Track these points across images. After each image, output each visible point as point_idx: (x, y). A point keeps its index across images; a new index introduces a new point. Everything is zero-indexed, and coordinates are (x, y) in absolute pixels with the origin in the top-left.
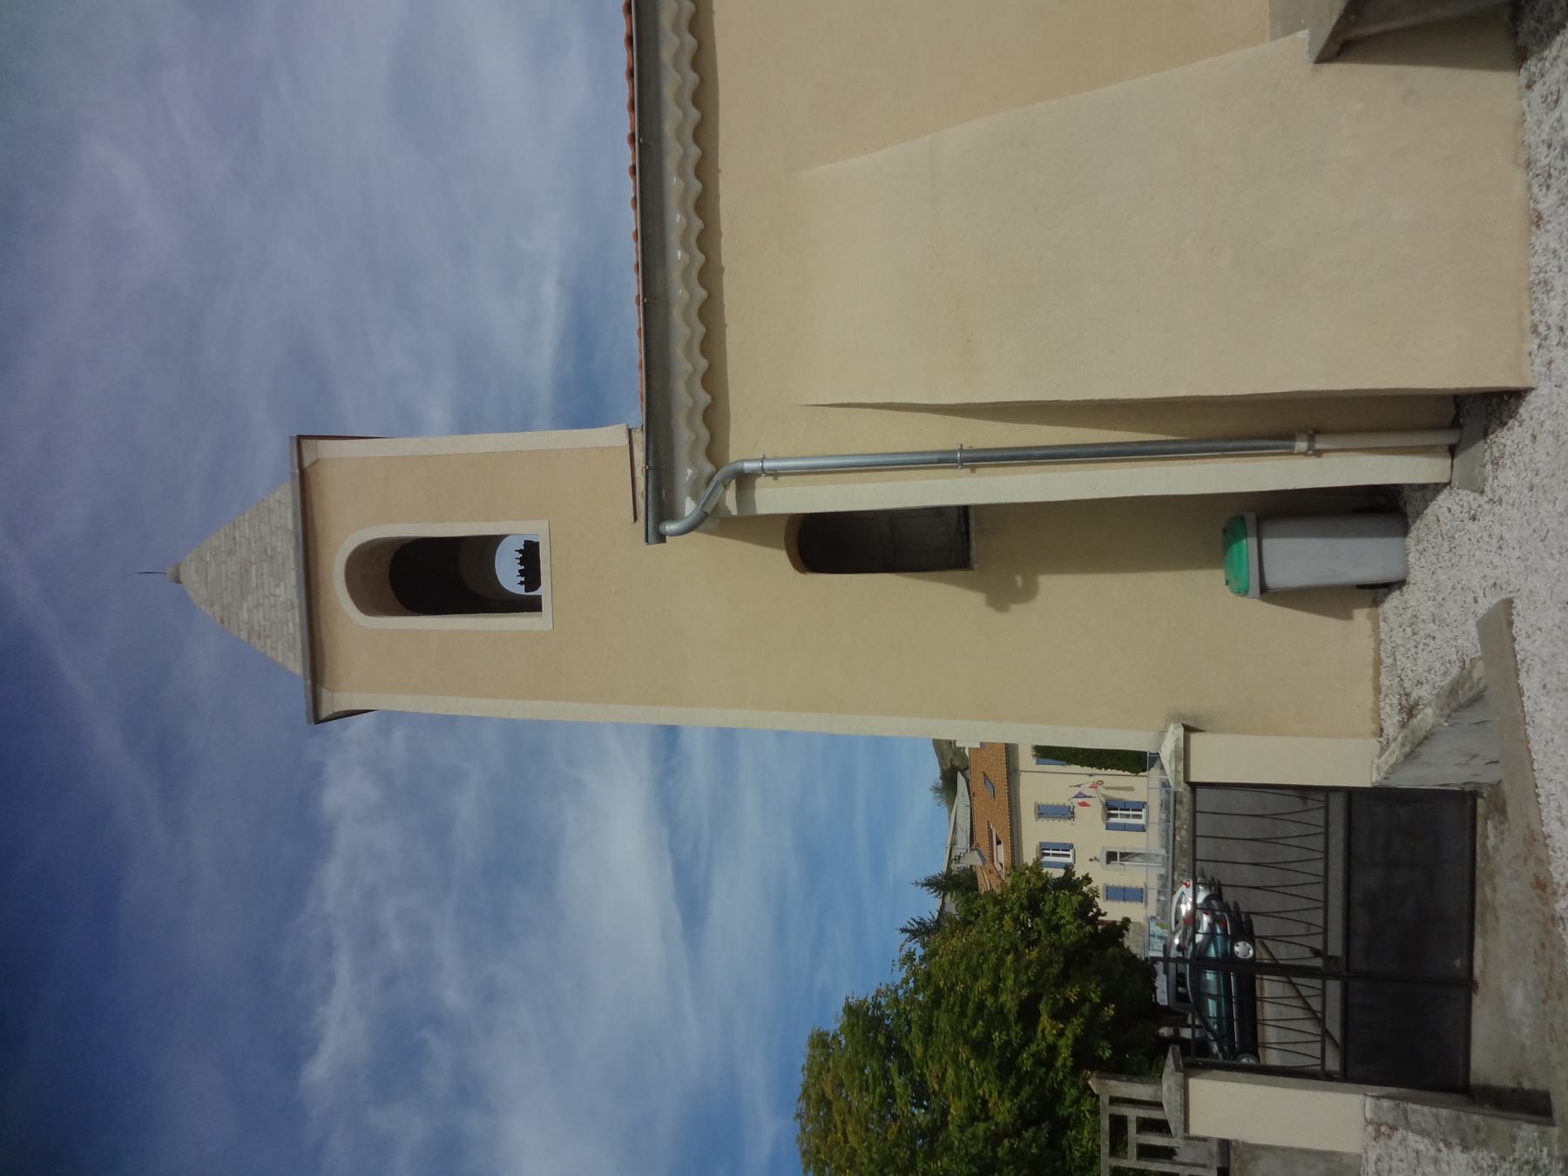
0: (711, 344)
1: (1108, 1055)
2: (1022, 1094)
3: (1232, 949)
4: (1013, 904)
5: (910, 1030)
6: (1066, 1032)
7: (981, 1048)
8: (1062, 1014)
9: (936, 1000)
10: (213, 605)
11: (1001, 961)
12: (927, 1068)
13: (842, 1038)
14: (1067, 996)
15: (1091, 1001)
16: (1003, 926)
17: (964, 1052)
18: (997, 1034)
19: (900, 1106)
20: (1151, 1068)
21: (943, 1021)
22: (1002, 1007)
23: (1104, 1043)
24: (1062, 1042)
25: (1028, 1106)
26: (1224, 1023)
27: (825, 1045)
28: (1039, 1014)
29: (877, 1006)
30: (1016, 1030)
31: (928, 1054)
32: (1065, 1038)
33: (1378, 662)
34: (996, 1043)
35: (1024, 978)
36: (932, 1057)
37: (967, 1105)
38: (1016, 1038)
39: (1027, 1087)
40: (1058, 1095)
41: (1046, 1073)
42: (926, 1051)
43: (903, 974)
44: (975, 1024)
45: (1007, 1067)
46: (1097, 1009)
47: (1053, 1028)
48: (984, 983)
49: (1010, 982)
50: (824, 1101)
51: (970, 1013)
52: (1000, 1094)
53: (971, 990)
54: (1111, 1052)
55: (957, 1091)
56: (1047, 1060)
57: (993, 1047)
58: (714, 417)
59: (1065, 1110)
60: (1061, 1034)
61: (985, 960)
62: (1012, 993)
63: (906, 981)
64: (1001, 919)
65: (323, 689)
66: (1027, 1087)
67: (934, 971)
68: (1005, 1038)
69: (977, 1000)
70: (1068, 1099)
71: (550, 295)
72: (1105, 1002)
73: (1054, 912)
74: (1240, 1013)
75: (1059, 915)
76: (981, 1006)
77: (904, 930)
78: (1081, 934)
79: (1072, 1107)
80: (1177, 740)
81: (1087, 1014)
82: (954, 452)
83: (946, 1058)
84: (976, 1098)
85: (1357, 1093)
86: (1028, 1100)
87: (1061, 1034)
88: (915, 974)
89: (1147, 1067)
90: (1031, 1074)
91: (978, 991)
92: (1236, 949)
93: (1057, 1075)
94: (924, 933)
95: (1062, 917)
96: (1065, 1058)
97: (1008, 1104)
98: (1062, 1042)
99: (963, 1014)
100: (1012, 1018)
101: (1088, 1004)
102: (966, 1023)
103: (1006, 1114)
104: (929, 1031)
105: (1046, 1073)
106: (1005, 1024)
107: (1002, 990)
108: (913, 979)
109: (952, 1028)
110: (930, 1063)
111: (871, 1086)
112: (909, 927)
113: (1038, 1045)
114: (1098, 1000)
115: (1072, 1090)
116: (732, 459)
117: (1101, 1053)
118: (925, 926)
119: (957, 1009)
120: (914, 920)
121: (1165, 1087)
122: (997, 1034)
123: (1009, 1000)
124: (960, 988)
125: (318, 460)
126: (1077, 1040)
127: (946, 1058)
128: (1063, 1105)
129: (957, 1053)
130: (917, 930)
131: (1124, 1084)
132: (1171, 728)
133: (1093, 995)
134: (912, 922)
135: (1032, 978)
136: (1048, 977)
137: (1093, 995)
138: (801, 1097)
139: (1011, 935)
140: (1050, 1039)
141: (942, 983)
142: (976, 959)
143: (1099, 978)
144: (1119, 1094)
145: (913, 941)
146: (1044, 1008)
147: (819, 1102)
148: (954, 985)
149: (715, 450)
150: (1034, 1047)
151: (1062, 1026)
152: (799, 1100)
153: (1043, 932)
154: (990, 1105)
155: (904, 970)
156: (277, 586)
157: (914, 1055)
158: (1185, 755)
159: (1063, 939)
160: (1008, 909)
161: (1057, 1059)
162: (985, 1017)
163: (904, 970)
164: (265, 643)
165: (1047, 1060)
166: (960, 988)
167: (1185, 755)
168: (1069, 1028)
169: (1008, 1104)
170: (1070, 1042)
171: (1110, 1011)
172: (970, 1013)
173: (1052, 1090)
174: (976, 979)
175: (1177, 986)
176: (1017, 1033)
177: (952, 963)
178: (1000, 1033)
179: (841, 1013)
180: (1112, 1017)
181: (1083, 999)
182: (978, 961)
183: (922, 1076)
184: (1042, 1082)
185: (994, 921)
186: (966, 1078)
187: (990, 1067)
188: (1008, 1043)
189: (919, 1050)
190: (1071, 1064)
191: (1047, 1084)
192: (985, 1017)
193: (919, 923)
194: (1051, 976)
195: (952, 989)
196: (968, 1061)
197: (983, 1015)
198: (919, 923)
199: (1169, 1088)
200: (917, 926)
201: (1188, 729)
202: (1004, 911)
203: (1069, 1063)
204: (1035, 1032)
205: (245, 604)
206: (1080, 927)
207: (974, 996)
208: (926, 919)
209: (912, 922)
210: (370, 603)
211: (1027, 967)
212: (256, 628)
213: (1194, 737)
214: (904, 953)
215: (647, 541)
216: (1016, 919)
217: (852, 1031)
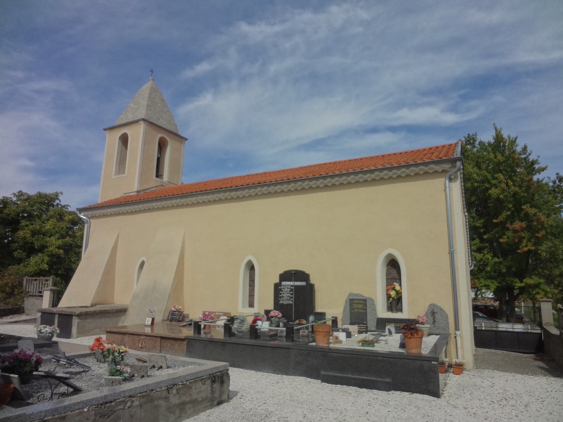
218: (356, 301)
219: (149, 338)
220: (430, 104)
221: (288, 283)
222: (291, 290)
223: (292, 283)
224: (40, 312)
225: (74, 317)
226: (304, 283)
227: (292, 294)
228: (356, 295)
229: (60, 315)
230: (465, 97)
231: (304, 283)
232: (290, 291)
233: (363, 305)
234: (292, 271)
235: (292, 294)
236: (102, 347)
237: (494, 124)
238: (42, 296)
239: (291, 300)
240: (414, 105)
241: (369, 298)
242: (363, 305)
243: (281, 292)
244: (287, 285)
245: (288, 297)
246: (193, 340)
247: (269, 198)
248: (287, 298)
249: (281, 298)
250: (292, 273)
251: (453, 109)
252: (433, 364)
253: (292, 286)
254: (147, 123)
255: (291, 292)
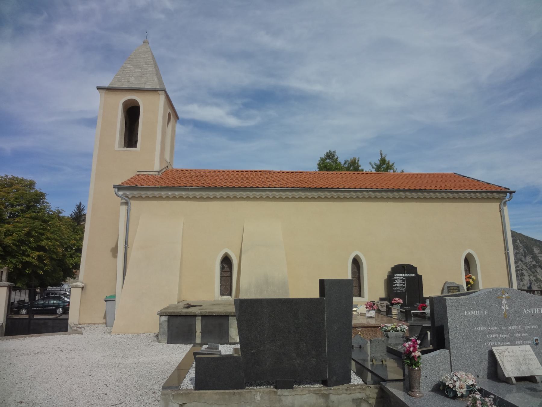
0: (154, 198)
1: (27, 272)
2: (14, 247)
3: (61, 308)
4: (80, 244)
5: (35, 212)
6: (34, 260)
7: (28, 234)
8: (40, 258)
9: (44, 221)
10: (134, 55)
11: (57, 241)
12: (22, 218)
13: (33, 191)
14: (46, 260)
15: (45, 267)
16: (72, 240)
17: (27, 230)
18: (33, 239)
19: (10, 209)
20: (23, 284)
21: (37, 223)
22: (42, 241)
23: (30, 271)
24: (30, 258)
25: (10, 248)
26: (36, 305)
27: (30, 185)
28: (39, 252)
29: (43, 203)
30: (35, 245)
31: (26, 218)
32: (32, 259)
33: (94, 324)
34: (30, 239)
35: (52, 247)
36: (25, 220)
37: (10, 230)
38: (32, 245)
39: (16, 248)
40: (14, 257)
41: (20, 254)
42: (28, 217)
43: (54, 210)
44: (36, 232)
45: (22, 242)
46: (42, 269)
47: (35, 256)
48: (50, 235)
49: (50, 243)
50: (11, 185)
51: (40, 231)
52: (14, 240)
53: (49, 232)
54: (28, 273)
55: (15, 227)
56: (24, 254)
57: (29, 238)
58: (140, 198)
59: (9, 259)
60: (33, 258)
61: (58, 236)
62: (47, 244)
63: (52, 211)
64: (75, 240)
65: (105, 91)
66: (16, 248)
67: (55, 221)
68: (32, 242)
69: (45, 233)
70: (12, 260)
71: (317, 88)
72: (44, 271)
73: (77, 256)
74: (40, 310)
75: (76, 257)
76: (42, 234)
77: (80, 204)
78: (69, 264)
79: (10, 261)
80: (80, 285)
81: (40, 266)
82: (127, 245)
83: (25, 224)
84: (13, 233)
85: (4, 321)
86: (12, 248)
87: (33, 258)
88: (54, 214)
89: (23, 283)
90: (20, 249)
91: (47, 234)
92: (60, 309)
93: (20, 257)
94: (79, 210)
95: (75, 259)
96: (25, 259)
97: (10, 242)
98: (30, 258)
99: (40, 229)
100: (39, 244)
101: (43, 266)
102: (37, 230)
103: (7, 242)
104: (35, 218)
105: (20, 254)
106: (36, 241)
107: (48, 241)
108: (52, 213)
109: (35, 226)
110: (23, 219)
111: (16, 200)
112: (82, 205)
113: (30, 251)
114: (45, 269)
115: (15, 261)
116: (131, 201)
117: (27, 270)
118: (82, 211)
119: (41, 227)
120: (84, 207)
121: (5, 282)
122: (33, 239)
123: (44, 243)
124: (49, 228)
125: (160, 95)
126: (32, 263)
127: (25, 224)
128: (11, 258)
129: (27, 227)
130: (80, 208)
131: (6, 274)
132: (83, 284)
133: (46, 268)
134: (83, 206)
135: (52, 250)
136: (52, 254)
137: (46, 268)
138: (13, 176)
139: (69, 243)
140: (32, 255)
141: (50, 222)
142: (58, 233)
143: (52, 270)
144: (3, 273)
145: (76, 207)
146: (41, 253)
147: (11, 183)
148: (50, 226)
149: (134, 198)
150: (29, 250)
151: (36, 258)
152: (12, 176)
153: (70, 253)
154: (10, 237)
155: (55, 211)
156: (134, 78)
157: (26, 214)
158: (76, 287)
159: (68, 259)
160: (78, 242)
161: (25, 257)
162: (39, 236)
163: (55, 211)
164: (121, 72)
165: (24, 254)
166: (49, 228)
167: (76, 287)
168: (35, 260)
169: (10, 242)
170: (31, 261)
171: (41, 272)
172: (40, 231)
173: (15, 255)
174: (52, 233)
175: (52, 293)
176: (33, 245)
177: (57, 226)
178: (33, 240)
179: (41, 191)
180: (39, 273)
181: (45, 265)
182: (57, 234)
183: (20, 216)
184: (18, 252)
185: (74, 238)
186: (19, 230)
187: (22, 237)
188: (30, 243)
189: (28, 215)
190: (23, 261)
191: (17, 254)
192: (39, 236)
193: (83, 209)
194: (52, 255)
195: (49, 225)
196: (24, 231)
197: (39, 235)
198: (83, 209)
199: (4, 283)
200: (82, 208)
201: (83, 288)
202: (77, 241)
203: (24, 260)
204: (34, 251)
205: (132, 66)
206: (72, 264)
207: (46, 233)
208: (85, 211)
209: (83, 206)
210: (125, 104)
211: (55, 248)
212: (125, 70)
213: (80, 289)
214: (61, 211)
215: (114, 185)
216: (74, 244)
217: (34, 195)
218: (452, 288)
219: (366, 329)
220: (217, 105)
221: (401, 275)
222: (403, 281)
223: (403, 275)
224: (166, 316)
225: (230, 318)
226: (414, 275)
227: (404, 284)
228: (451, 283)
229: (205, 317)
230: (247, 106)
231: (414, 275)
232: (402, 282)
233: (457, 290)
234: (404, 265)
235: (404, 284)
236: (379, 340)
237: (381, 151)
238: (115, 300)
239: (404, 289)
240: (204, 103)
241: (461, 285)
242: (457, 290)
243: (394, 283)
244: (399, 277)
245: (401, 286)
246: (415, 326)
247: (362, 201)
248: (399, 287)
249: (395, 287)
250: (404, 267)
251: (236, 114)
252: (427, 333)
253: (404, 277)
254: (104, 91)
255: (403, 283)
